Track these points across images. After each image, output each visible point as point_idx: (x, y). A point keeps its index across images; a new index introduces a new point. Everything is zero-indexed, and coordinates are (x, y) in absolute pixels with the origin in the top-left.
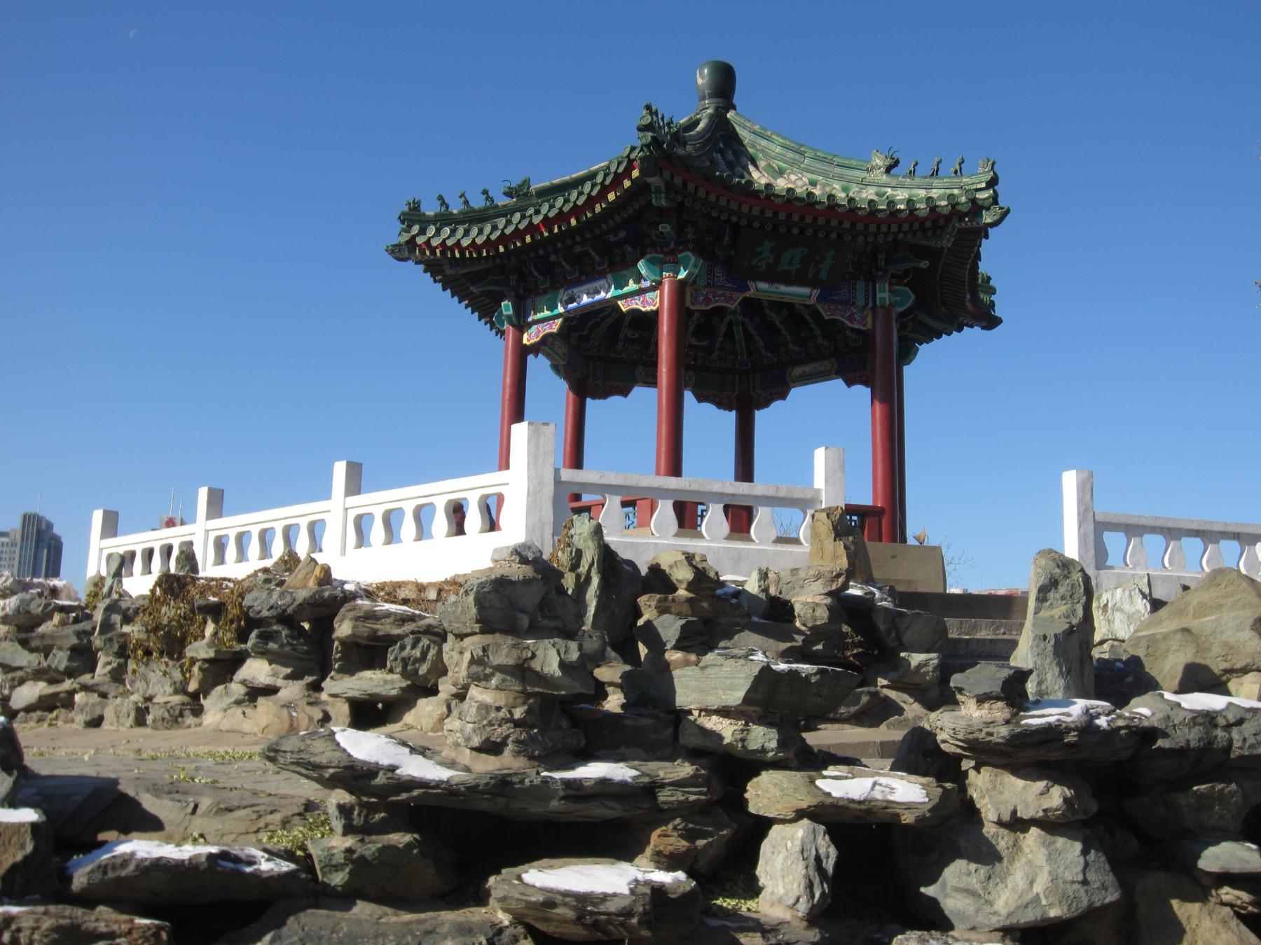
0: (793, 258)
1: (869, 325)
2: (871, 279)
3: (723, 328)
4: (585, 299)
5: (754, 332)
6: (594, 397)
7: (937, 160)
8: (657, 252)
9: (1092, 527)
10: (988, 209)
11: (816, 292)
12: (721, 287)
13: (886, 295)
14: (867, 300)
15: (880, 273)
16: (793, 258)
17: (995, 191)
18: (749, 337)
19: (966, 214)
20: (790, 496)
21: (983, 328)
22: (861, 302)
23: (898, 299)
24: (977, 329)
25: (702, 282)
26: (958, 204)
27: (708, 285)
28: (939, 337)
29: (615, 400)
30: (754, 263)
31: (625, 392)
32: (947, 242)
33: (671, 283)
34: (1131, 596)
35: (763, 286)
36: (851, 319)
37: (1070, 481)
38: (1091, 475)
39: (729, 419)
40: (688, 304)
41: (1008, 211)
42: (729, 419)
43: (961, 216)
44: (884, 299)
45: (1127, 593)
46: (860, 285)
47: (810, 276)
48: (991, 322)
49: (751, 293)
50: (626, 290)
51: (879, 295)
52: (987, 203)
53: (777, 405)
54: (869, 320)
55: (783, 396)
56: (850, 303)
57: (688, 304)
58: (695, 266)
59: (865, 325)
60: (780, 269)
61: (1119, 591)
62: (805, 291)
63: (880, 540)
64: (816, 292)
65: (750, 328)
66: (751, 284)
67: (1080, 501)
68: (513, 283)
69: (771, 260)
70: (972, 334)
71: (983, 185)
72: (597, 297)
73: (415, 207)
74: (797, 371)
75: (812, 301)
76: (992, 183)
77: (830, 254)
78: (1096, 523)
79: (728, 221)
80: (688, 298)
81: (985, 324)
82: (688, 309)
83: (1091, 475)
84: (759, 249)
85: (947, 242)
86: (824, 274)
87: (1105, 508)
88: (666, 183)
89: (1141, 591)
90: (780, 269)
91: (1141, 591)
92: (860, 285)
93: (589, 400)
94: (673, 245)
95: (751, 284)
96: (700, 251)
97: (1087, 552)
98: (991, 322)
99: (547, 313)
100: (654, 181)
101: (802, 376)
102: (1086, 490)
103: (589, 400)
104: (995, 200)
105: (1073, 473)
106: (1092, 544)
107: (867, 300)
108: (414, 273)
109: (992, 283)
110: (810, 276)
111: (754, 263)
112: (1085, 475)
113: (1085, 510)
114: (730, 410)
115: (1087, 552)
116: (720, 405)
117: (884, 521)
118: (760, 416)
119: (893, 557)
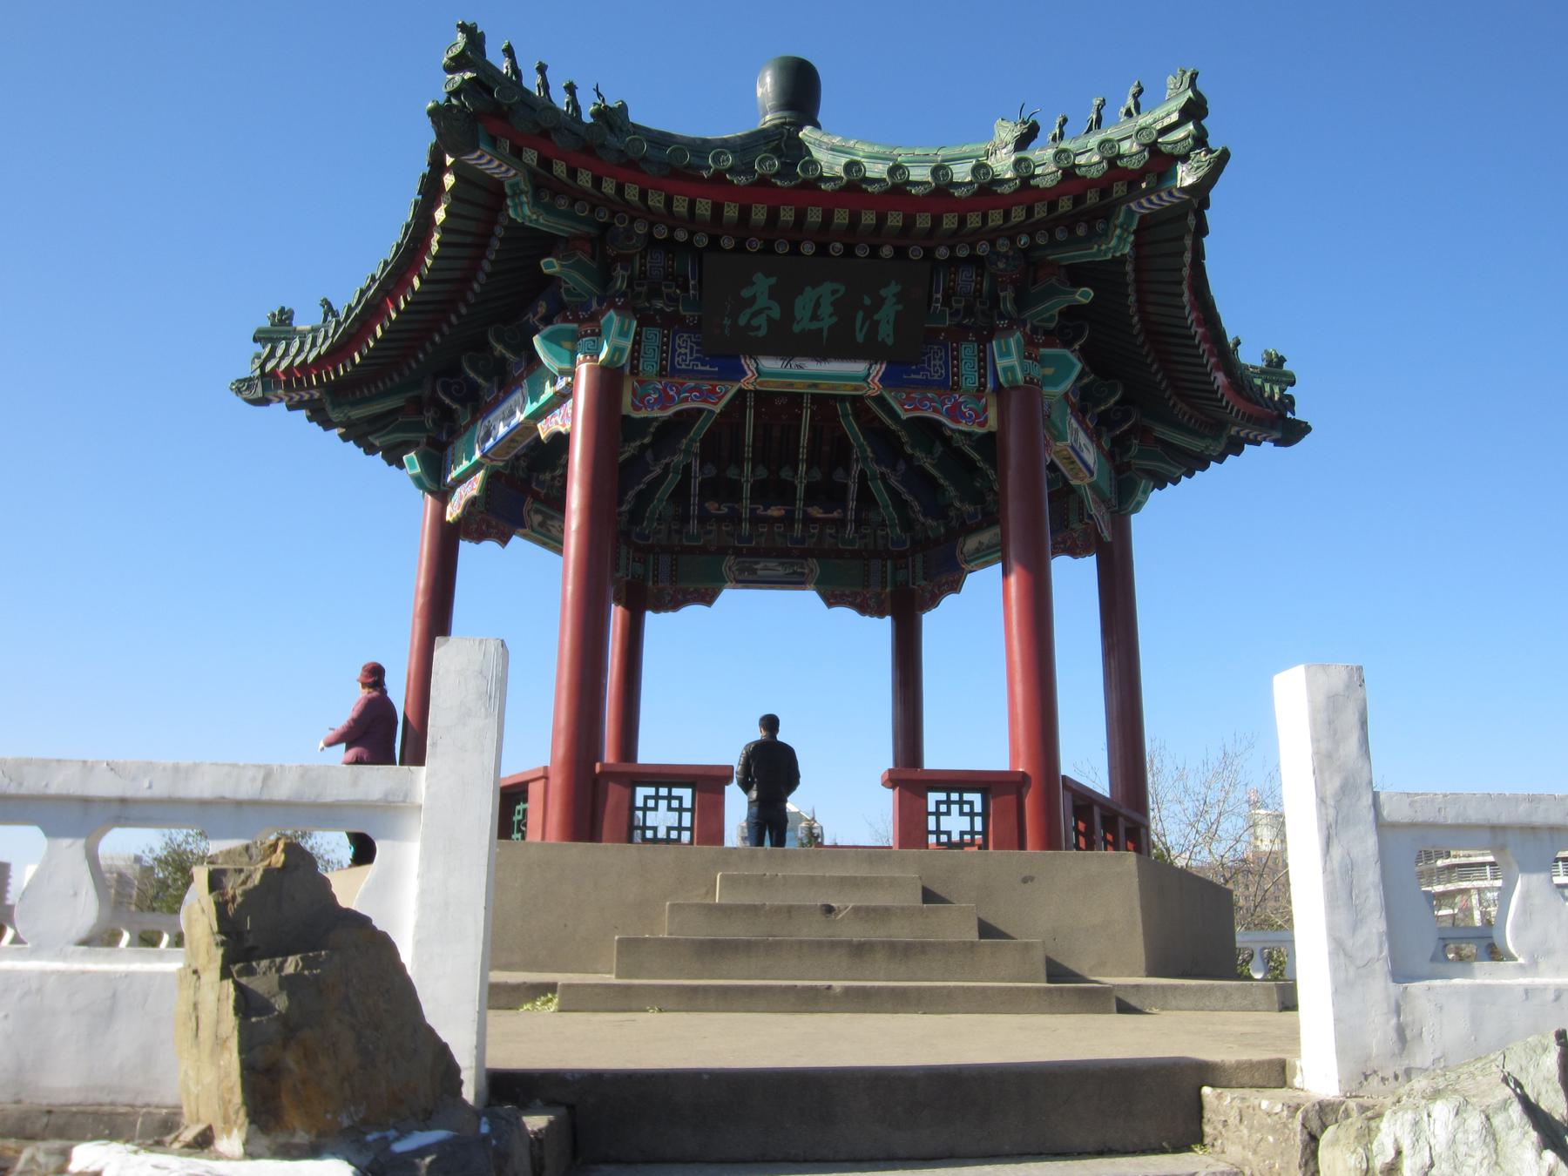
0: (817, 305)
1: (993, 423)
2: (985, 336)
3: (853, 488)
4: (502, 430)
5: (901, 489)
6: (658, 608)
7: (1097, 102)
8: (566, 320)
9: (1371, 842)
10: (1185, 158)
11: (879, 369)
12: (691, 373)
13: (1014, 361)
14: (983, 376)
15: (1003, 323)
16: (817, 305)
17: (1198, 126)
18: (900, 505)
19: (1141, 174)
20: (309, 795)
21: (1277, 443)
22: (969, 379)
23: (1049, 371)
24: (1267, 446)
25: (649, 366)
26: (1120, 156)
27: (662, 373)
28: (1204, 466)
29: (693, 611)
30: (742, 321)
31: (707, 598)
32: (1118, 244)
33: (590, 369)
34: (1490, 1133)
35: (770, 364)
36: (955, 413)
37: (1293, 696)
38: (1358, 677)
39: (881, 629)
40: (627, 407)
41: (1224, 156)
42: (881, 629)
43: (1132, 179)
44: (1011, 369)
45: (1475, 1121)
46: (968, 351)
47: (860, 337)
48: (1290, 432)
49: (748, 383)
50: (544, 398)
51: (1001, 363)
52: (1180, 150)
53: (949, 601)
54: (992, 414)
55: (955, 587)
56: (948, 385)
57: (627, 407)
58: (623, 333)
59: (982, 425)
60: (797, 328)
61: (1442, 1110)
62: (859, 367)
63: (1022, 845)
64: (879, 369)
65: (893, 482)
66: (748, 365)
67: (1325, 761)
68: (429, 424)
69: (776, 313)
70: (1260, 457)
71: (1175, 117)
72: (514, 422)
73: (284, 318)
74: (971, 543)
75: (875, 388)
76: (1194, 110)
77: (890, 291)
78: (1383, 827)
79: (689, 244)
80: (627, 398)
81: (1277, 435)
82: (627, 418)
83: (1358, 677)
84: (746, 293)
85: (1118, 244)
86: (886, 333)
87: (1428, 770)
88: (533, 175)
89: (1533, 1111)
90: (797, 328)
91: (1533, 1111)
92: (968, 351)
93: (650, 618)
94: (595, 305)
95: (748, 365)
96: (629, 308)
97: (1355, 926)
98: (1290, 432)
99: (466, 464)
100: (486, 162)
101: (978, 550)
102: (1347, 721)
103: (650, 618)
104: (1200, 140)
105: (1300, 671)
106: (1373, 898)
107: (983, 376)
108: (288, 425)
109: (1286, 367)
110: (860, 337)
111: (742, 321)
112: (1337, 678)
113: (1346, 789)
114: (881, 614)
115: (1355, 926)
116: (865, 608)
117: (1029, 802)
118: (931, 622)
119: (1025, 880)
